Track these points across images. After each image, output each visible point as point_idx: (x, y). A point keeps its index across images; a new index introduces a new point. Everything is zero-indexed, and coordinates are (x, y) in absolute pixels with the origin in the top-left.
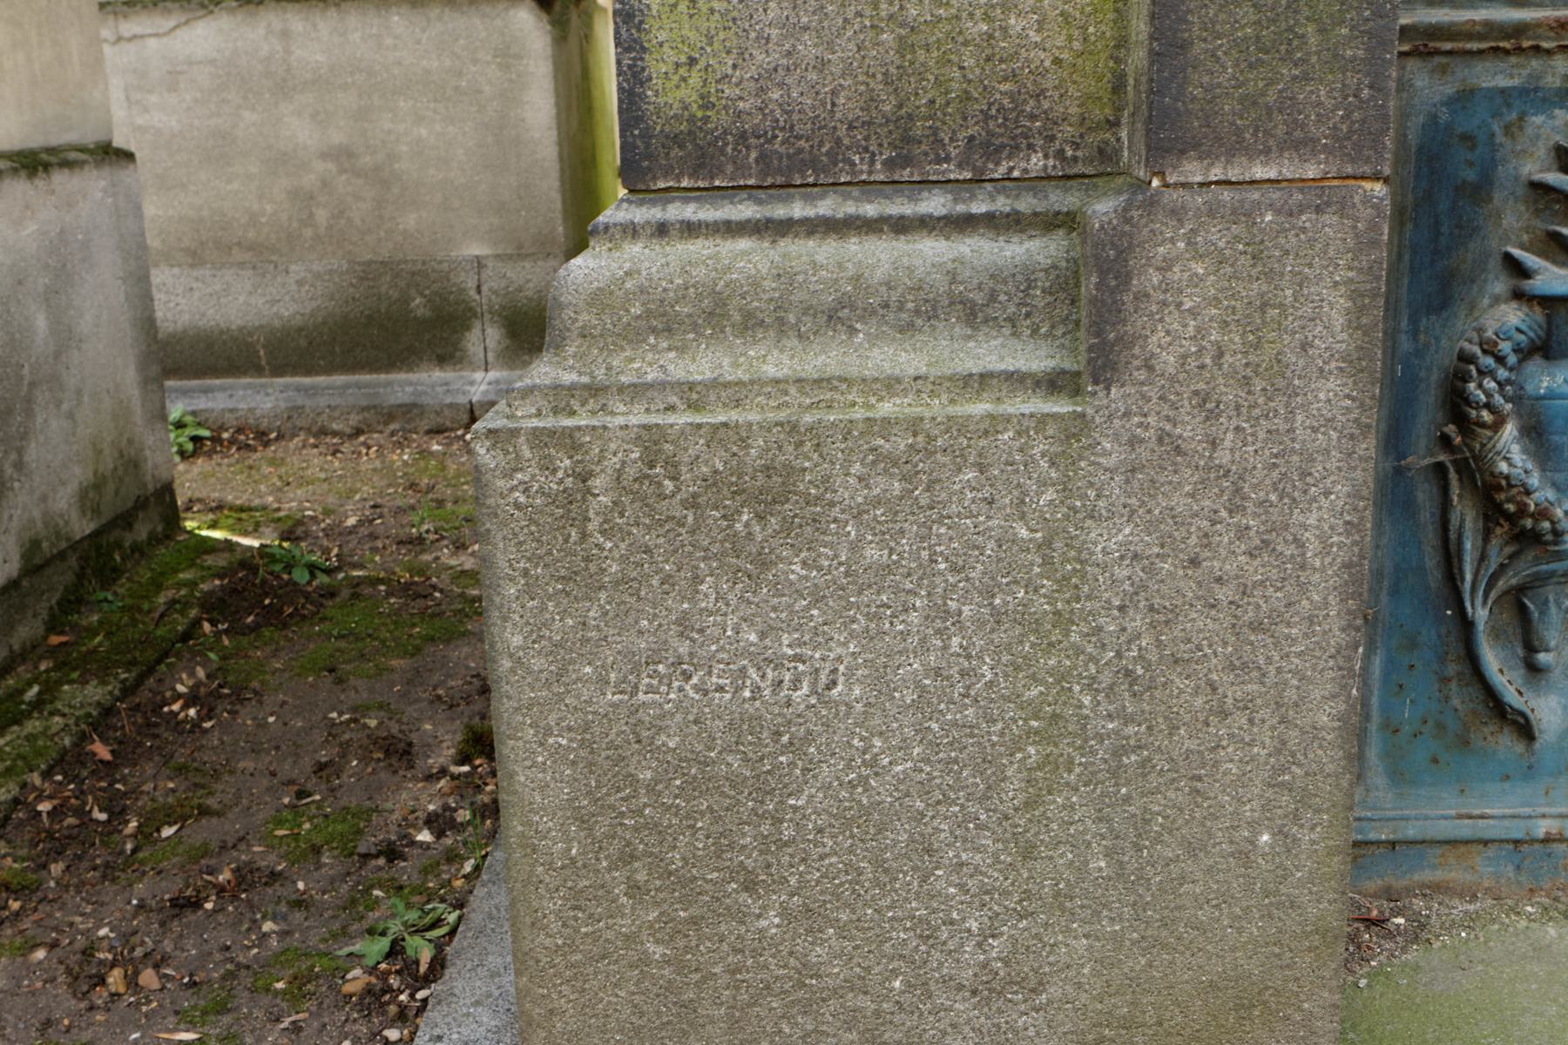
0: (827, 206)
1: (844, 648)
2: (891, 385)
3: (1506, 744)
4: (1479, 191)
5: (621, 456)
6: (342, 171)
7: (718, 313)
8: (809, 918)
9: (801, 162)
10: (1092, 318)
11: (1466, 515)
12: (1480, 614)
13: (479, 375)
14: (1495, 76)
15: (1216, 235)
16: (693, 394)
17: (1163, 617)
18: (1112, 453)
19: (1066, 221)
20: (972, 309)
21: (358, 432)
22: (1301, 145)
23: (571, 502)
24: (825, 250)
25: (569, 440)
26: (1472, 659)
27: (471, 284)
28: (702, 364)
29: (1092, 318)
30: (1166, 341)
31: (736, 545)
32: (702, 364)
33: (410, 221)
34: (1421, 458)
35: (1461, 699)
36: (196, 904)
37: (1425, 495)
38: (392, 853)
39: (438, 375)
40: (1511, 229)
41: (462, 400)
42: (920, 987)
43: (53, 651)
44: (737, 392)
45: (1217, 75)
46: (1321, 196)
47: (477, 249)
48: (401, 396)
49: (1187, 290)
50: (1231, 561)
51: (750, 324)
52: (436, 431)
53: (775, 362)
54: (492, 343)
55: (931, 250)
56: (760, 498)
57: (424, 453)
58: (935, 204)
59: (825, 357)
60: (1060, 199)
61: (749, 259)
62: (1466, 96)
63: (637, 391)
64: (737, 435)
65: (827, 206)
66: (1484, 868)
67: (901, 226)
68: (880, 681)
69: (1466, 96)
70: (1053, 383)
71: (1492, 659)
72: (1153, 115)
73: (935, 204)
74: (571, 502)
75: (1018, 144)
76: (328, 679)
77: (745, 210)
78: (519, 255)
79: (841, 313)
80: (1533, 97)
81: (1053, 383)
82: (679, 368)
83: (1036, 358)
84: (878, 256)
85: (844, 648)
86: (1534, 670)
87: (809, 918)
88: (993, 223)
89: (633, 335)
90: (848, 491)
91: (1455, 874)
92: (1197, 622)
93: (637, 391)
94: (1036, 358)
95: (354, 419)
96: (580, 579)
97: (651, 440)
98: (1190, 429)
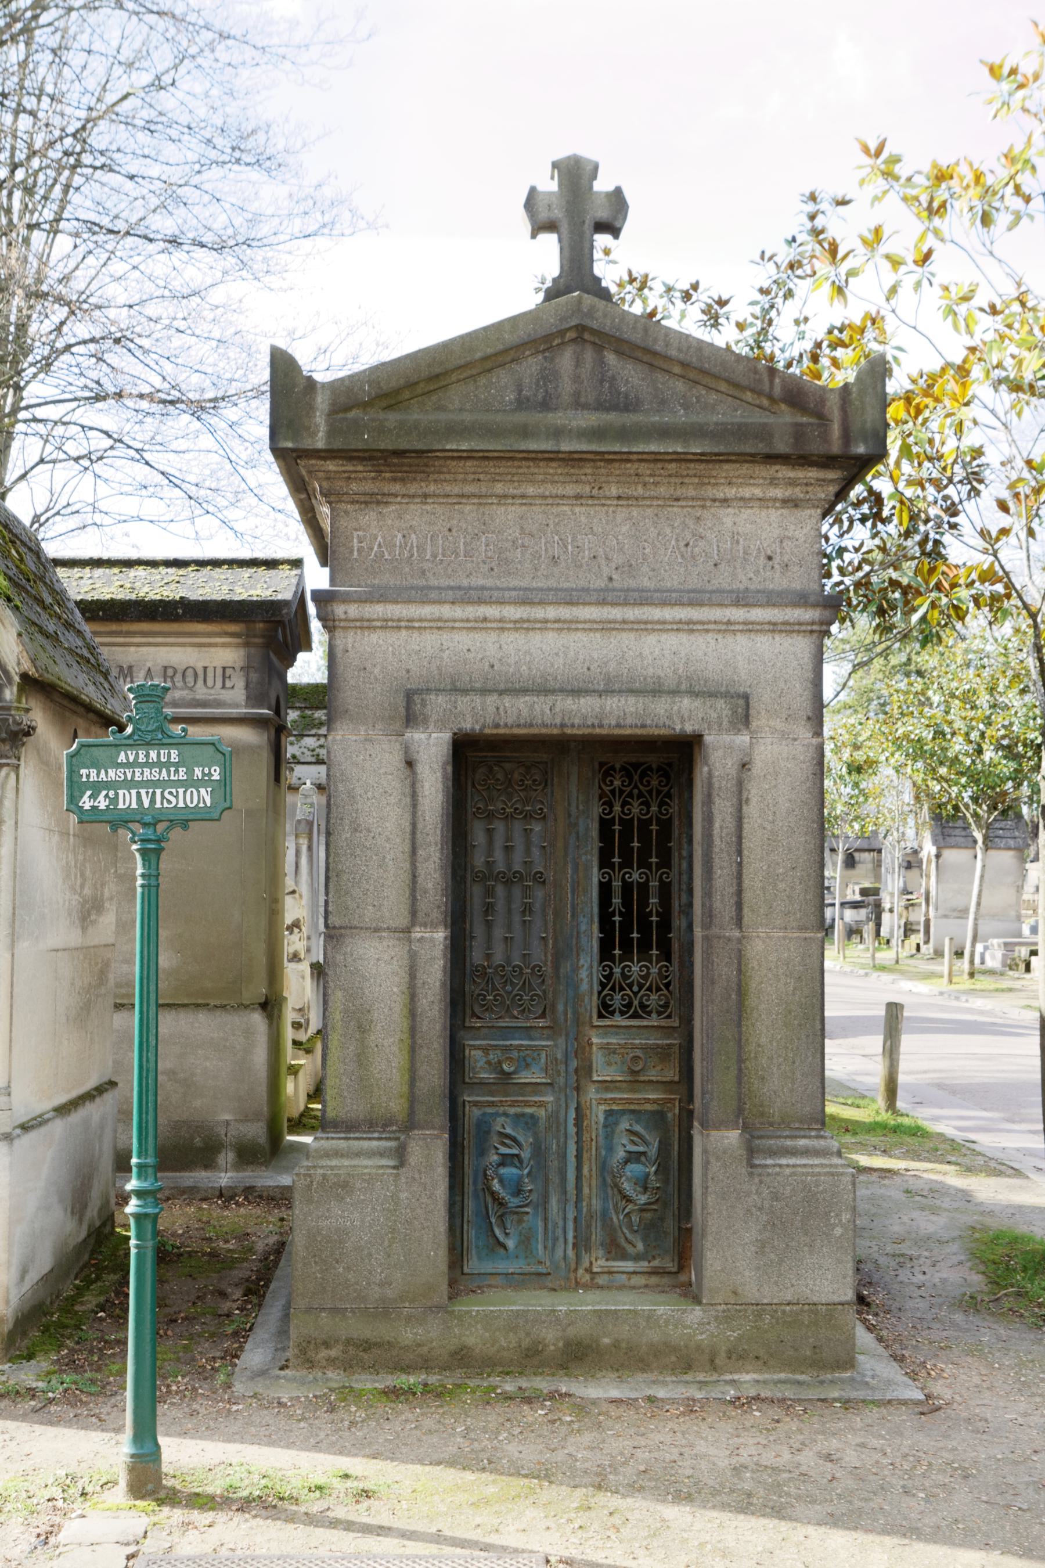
0: (357, 1135)
1: (356, 1215)
2: (366, 1167)
3: (502, 1251)
4: (488, 1132)
5: (319, 1178)
6: (170, 1080)
7: (337, 1154)
8: (348, 1269)
9: (352, 1127)
10: (400, 1155)
11: (489, 1200)
12: (493, 1221)
13: (223, 1175)
14: (490, 1110)
15: (420, 1143)
16: (332, 1168)
17: (413, 1210)
18: (403, 1180)
19: (398, 1139)
20: (381, 1154)
21: (168, 1199)
22: (433, 1128)
23: (309, 1187)
24: (356, 1143)
25: (310, 1176)
26: (493, 1231)
27: (223, 1132)
28: (334, 1163)
29: (400, 1155)
30: (412, 1160)
31: (338, 1195)
32: (334, 1163)
33: (198, 1103)
34: (480, 1186)
35: (491, 1241)
36: (176, 1321)
37: (481, 1194)
38: (228, 1316)
39: (203, 1174)
40: (495, 1140)
41: (216, 1185)
42: (368, 1284)
43: (93, 1265)
44: (339, 1168)
45: (420, 1116)
46: (437, 1137)
47: (227, 1117)
48: (189, 1183)
49: (416, 1152)
50: (424, 1200)
51: (342, 1156)
52: (204, 1199)
53: (346, 1163)
54: (229, 1160)
55: (375, 1143)
56: (343, 1186)
57: (200, 1209)
58: (376, 1135)
59: (355, 1162)
60: (398, 1135)
61: (343, 1144)
62: (484, 1114)
63: (322, 1167)
64: (339, 1175)
65: (357, 1135)
66: (498, 1281)
67: (370, 1139)
68: (363, 1221)
69: (484, 1114)
70: (394, 1167)
71: (497, 1232)
72: (410, 1124)
73: (376, 1135)
74: (309, 1187)
75: (391, 1125)
76: (189, 1279)
77: (343, 1135)
78: (245, 1120)
79: (358, 1154)
80: (497, 1115)
81: (394, 1167)
82: (329, 1163)
83: (392, 1163)
84: (365, 1144)
85: (356, 1215)
86: (507, 1234)
87: (348, 1269)
88: (386, 1139)
89: (321, 1157)
90: (358, 1186)
91: (493, 1282)
92: (419, 1211)
93: (322, 1167)
94: (392, 1163)
95: (167, 1193)
96: (310, 1201)
97: (324, 1176)
98: (417, 1176)
